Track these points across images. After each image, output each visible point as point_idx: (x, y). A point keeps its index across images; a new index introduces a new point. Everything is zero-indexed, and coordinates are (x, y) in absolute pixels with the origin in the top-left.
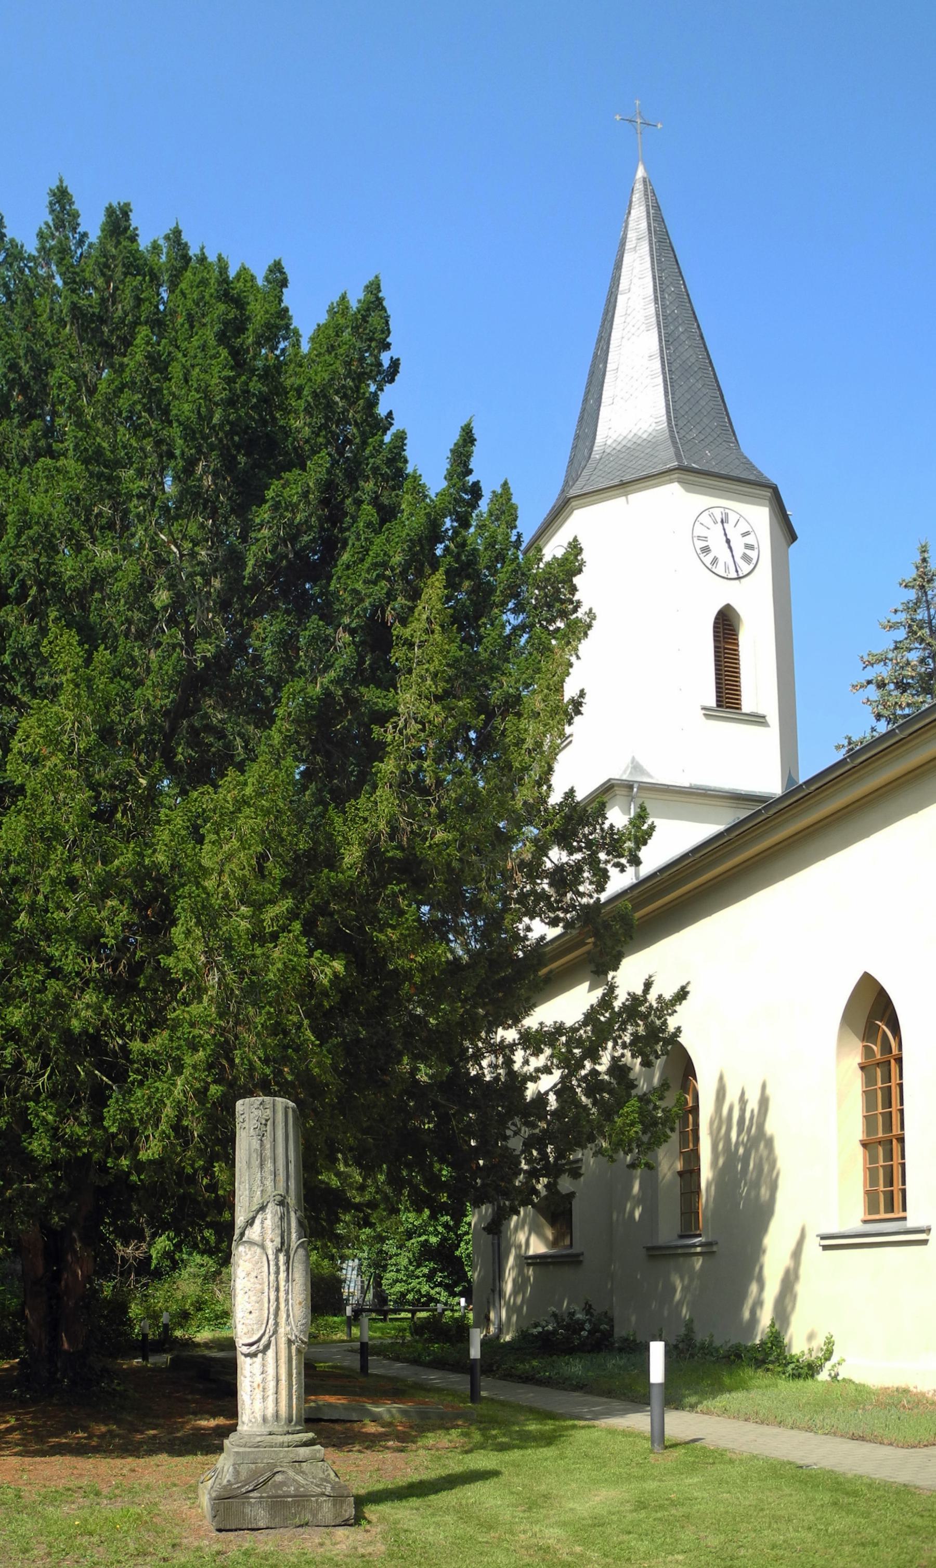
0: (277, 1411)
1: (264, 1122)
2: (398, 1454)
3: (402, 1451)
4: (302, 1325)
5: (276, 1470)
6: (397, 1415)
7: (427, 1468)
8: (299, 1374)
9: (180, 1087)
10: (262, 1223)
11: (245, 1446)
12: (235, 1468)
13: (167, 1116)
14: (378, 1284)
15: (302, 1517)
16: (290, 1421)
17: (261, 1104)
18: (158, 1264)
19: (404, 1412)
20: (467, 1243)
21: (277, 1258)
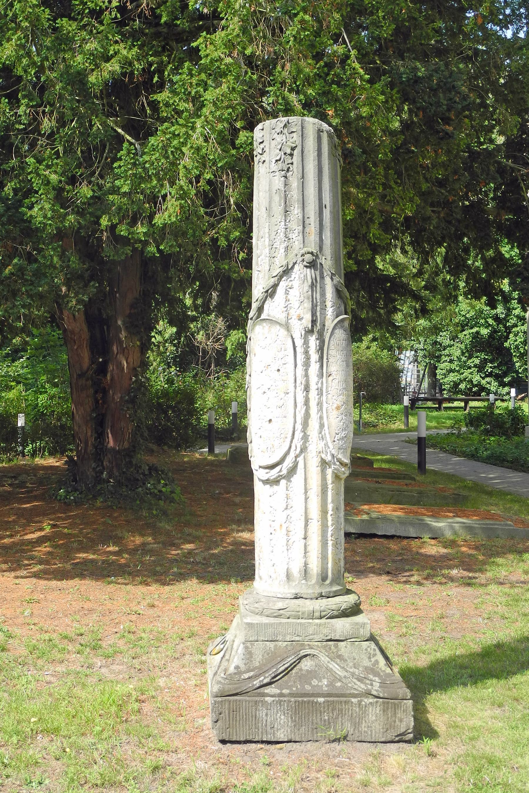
0: (306, 564)
1: (289, 151)
2: (464, 590)
3: (469, 585)
4: (342, 439)
5: (302, 653)
6: (460, 531)
7: (504, 618)
8: (336, 509)
9: (199, 130)
10: (287, 292)
11: (261, 614)
12: (246, 648)
13: (185, 167)
14: (433, 373)
15: (338, 726)
16: (324, 578)
17: (285, 126)
18: (233, 355)
19: (469, 529)
20: (516, 335)
21: (306, 343)
